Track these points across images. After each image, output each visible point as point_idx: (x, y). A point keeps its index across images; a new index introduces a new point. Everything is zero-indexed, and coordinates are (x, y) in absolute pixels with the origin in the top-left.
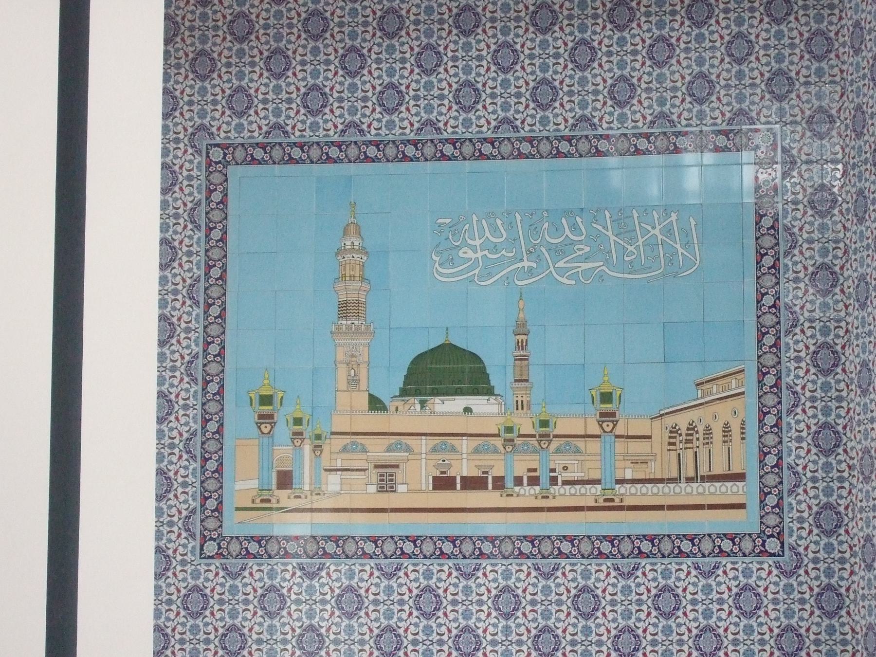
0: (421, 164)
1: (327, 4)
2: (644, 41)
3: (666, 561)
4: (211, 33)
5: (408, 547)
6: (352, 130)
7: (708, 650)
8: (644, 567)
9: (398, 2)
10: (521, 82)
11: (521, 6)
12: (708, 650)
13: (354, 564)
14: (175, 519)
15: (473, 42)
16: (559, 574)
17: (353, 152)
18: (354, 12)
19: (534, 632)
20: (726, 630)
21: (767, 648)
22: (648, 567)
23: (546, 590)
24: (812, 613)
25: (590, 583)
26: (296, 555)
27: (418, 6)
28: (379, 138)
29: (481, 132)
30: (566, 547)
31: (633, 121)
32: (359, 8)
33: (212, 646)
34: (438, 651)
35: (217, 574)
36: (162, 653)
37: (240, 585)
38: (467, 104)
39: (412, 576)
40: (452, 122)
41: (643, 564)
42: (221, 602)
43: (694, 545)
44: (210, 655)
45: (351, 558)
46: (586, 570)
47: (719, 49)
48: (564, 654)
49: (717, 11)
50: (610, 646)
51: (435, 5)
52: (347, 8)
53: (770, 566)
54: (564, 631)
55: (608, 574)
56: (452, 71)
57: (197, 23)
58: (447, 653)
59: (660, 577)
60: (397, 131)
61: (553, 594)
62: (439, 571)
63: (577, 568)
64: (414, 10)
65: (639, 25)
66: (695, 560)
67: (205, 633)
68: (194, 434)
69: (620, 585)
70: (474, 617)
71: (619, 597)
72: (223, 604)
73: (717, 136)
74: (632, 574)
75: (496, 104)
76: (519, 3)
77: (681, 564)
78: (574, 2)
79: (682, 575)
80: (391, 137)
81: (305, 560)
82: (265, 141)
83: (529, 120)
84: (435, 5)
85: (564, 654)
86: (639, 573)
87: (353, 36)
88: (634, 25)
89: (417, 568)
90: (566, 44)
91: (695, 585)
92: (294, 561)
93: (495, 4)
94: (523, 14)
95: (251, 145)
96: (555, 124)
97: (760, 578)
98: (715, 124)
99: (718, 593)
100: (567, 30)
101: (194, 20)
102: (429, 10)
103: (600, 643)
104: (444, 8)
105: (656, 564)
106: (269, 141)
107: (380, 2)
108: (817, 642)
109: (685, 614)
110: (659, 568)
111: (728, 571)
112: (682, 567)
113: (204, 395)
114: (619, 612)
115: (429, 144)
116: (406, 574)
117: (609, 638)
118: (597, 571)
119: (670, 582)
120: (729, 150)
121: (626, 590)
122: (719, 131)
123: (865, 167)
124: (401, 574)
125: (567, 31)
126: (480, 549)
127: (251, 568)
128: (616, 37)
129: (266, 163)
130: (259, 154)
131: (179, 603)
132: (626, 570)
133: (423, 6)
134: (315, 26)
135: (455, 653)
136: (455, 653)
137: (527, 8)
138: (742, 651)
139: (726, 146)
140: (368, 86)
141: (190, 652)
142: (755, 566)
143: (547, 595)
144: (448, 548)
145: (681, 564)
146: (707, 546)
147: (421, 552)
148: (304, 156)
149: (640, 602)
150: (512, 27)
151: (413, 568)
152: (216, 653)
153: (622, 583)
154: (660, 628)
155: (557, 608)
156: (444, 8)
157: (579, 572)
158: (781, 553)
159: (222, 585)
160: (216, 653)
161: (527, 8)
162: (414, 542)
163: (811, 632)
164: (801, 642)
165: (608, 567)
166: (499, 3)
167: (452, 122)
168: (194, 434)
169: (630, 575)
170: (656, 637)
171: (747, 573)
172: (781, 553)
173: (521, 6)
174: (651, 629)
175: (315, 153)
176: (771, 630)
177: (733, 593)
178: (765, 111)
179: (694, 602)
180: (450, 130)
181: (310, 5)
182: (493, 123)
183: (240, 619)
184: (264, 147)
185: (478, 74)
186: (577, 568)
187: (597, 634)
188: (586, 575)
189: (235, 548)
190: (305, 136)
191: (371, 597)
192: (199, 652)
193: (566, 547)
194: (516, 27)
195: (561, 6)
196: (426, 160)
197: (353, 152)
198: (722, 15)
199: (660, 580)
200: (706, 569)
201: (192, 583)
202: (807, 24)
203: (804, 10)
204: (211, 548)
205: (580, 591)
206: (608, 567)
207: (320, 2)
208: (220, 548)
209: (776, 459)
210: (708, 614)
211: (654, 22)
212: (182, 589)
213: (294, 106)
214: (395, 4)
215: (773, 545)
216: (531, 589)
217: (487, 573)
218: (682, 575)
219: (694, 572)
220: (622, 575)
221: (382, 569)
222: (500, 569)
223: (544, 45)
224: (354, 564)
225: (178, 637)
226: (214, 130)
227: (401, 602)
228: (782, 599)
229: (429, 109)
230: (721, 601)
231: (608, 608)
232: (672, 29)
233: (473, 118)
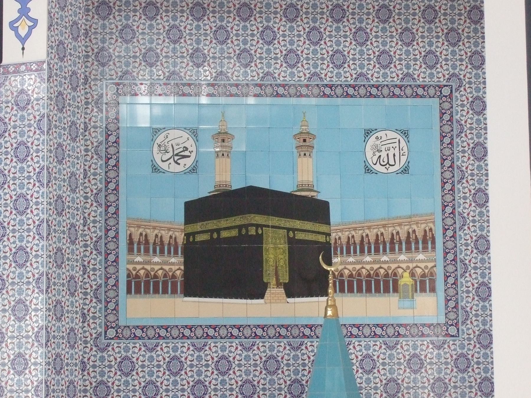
0: (381, 99)
1: (436, 2)
2: (285, 382)
3: (223, 341)
4: (457, 18)
5: (211, 332)
6: (315, 77)
7: (296, 394)
8: (354, 343)
9: (388, 1)
10: (324, 51)
11: (184, 4)
12: (296, 394)
13: (178, 343)
14: (91, 370)
15: (341, 26)
16: (110, 349)
17: (409, 91)
18: (407, 7)
19: (288, 383)
20: (162, 383)
21: (283, 392)
22: (213, 345)
23: (199, 358)
24: (261, 372)
25: (129, 354)
26: (428, 336)
27: (308, 3)
28: (425, 83)
29: (347, 81)
31: (298, 77)
32: (410, 4)
33: (379, 391)
34: (230, 395)
35: (189, 349)
36: (396, 395)
37: (106, 356)
39: (358, 348)
40: (329, 74)
41: (306, 342)
42: (207, 366)
43: (191, 332)
44: (378, 396)
45: (127, 339)
46: (126, 346)
47: (162, 34)
48: (259, 396)
49: (161, 11)
50: (286, 391)
51: (318, 3)
52: (449, 5)
53: (140, 345)
54: (162, 383)
55: (140, 349)
56: (236, 43)
57: (449, 11)
58: (284, 395)
60: (389, 79)
61: (300, 360)
62: (374, 345)
63: (218, 344)
64: (305, 6)
65: (161, 18)
66: (240, 340)
67: (469, 382)
69: (243, 355)
70: (106, 375)
71: (243, 362)
72: (192, 367)
73: (255, 87)
74: (299, 348)
75: (356, 64)
76: (183, 2)
77: (232, 342)
78: (122, 2)
79: (136, 350)
80: (339, 83)
81: (434, 338)
82: (401, 83)
83: (329, 74)
84: (318, 3)
85: (259, 396)
86: (207, 348)
87: (407, 21)
88: (206, 18)
89: (217, 345)
90: (304, 29)
92: (428, 339)
93: (261, 3)
94: (232, 9)
95: (346, 86)
96: (345, 77)
98: (112, 79)
99: (157, 361)
100: (305, 21)
101: (215, 7)
102: (315, 6)
103: (231, 390)
104: (324, 5)
105: (169, 343)
107: (423, 1)
108: (215, 390)
109: (137, 373)
110: (171, 345)
112: (377, 343)
114: (146, 372)
115: (339, 87)
116: (113, 349)
117: (189, 387)
118: (374, 345)
119: (197, 354)
120: (262, 96)
121: (247, 358)
122: (256, 84)
124: (207, 348)
125: (259, 20)
126: (374, 332)
127: (162, 345)
128: (288, 26)
129: (379, 97)
130: (351, 91)
131: (186, 366)
132: (296, 346)
133: (311, 3)
134: (383, 14)
135: (288, 396)
136: (288, 396)
137: (188, 5)
138: (268, 395)
139: (213, 93)
141: (365, 395)
142: (276, 345)
143: (200, 361)
144: (187, 332)
145: (280, 342)
146: (199, 332)
148: (379, 93)
149: (256, 365)
150: (365, 19)
151: (262, 344)
152: (381, 395)
153: (245, 353)
154: (122, 382)
156: (324, 5)
158: (457, 335)
159: (384, 354)
160: (381, 395)
161: (188, 5)
162: (239, 329)
163: (212, 384)
164: (158, 391)
165: (285, 344)
166: (218, 2)
167: (329, 74)
169: (249, 349)
170: (120, 387)
171: (367, 348)
172: (457, 335)
173: (184, 4)
174: (117, 383)
175: (386, 91)
176: (476, 380)
178: (141, 72)
179: (94, 366)
180: (328, 79)
181: (472, 2)
182: (354, 76)
183: (106, 377)
184: (354, 87)
185: (298, 46)
186: (218, 344)
187: (278, 384)
188: (127, 350)
190: (426, 81)
191: (475, 360)
192: (371, 395)
193: (163, 333)
194: (274, 18)
195: (114, 4)
196: (384, 97)
197: (409, 91)
198: (117, 13)
199: (220, 352)
200: (248, 346)
201: (394, 352)
202: (168, 21)
203: (306, 15)
204: (452, 330)
206: (189, 345)
207: (477, 1)
209: (454, 279)
210: (247, 373)
211: (310, 18)
212: (359, 356)
214: (386, 3)
215: (111, 333)
216: (476, 355)
217: (212, 348)
219: (288, 347)
220: (293, 348)
221: (434, 344)
222: (411, 343)
223: (245, 28)
224: (178, 343)
225: (261, 386)
226: (416, 76)
227: (159, 366)
229: (315, 66)
230: (240, 365)
231: (189, 369)
232: (228, 22)
233: (296, 72)
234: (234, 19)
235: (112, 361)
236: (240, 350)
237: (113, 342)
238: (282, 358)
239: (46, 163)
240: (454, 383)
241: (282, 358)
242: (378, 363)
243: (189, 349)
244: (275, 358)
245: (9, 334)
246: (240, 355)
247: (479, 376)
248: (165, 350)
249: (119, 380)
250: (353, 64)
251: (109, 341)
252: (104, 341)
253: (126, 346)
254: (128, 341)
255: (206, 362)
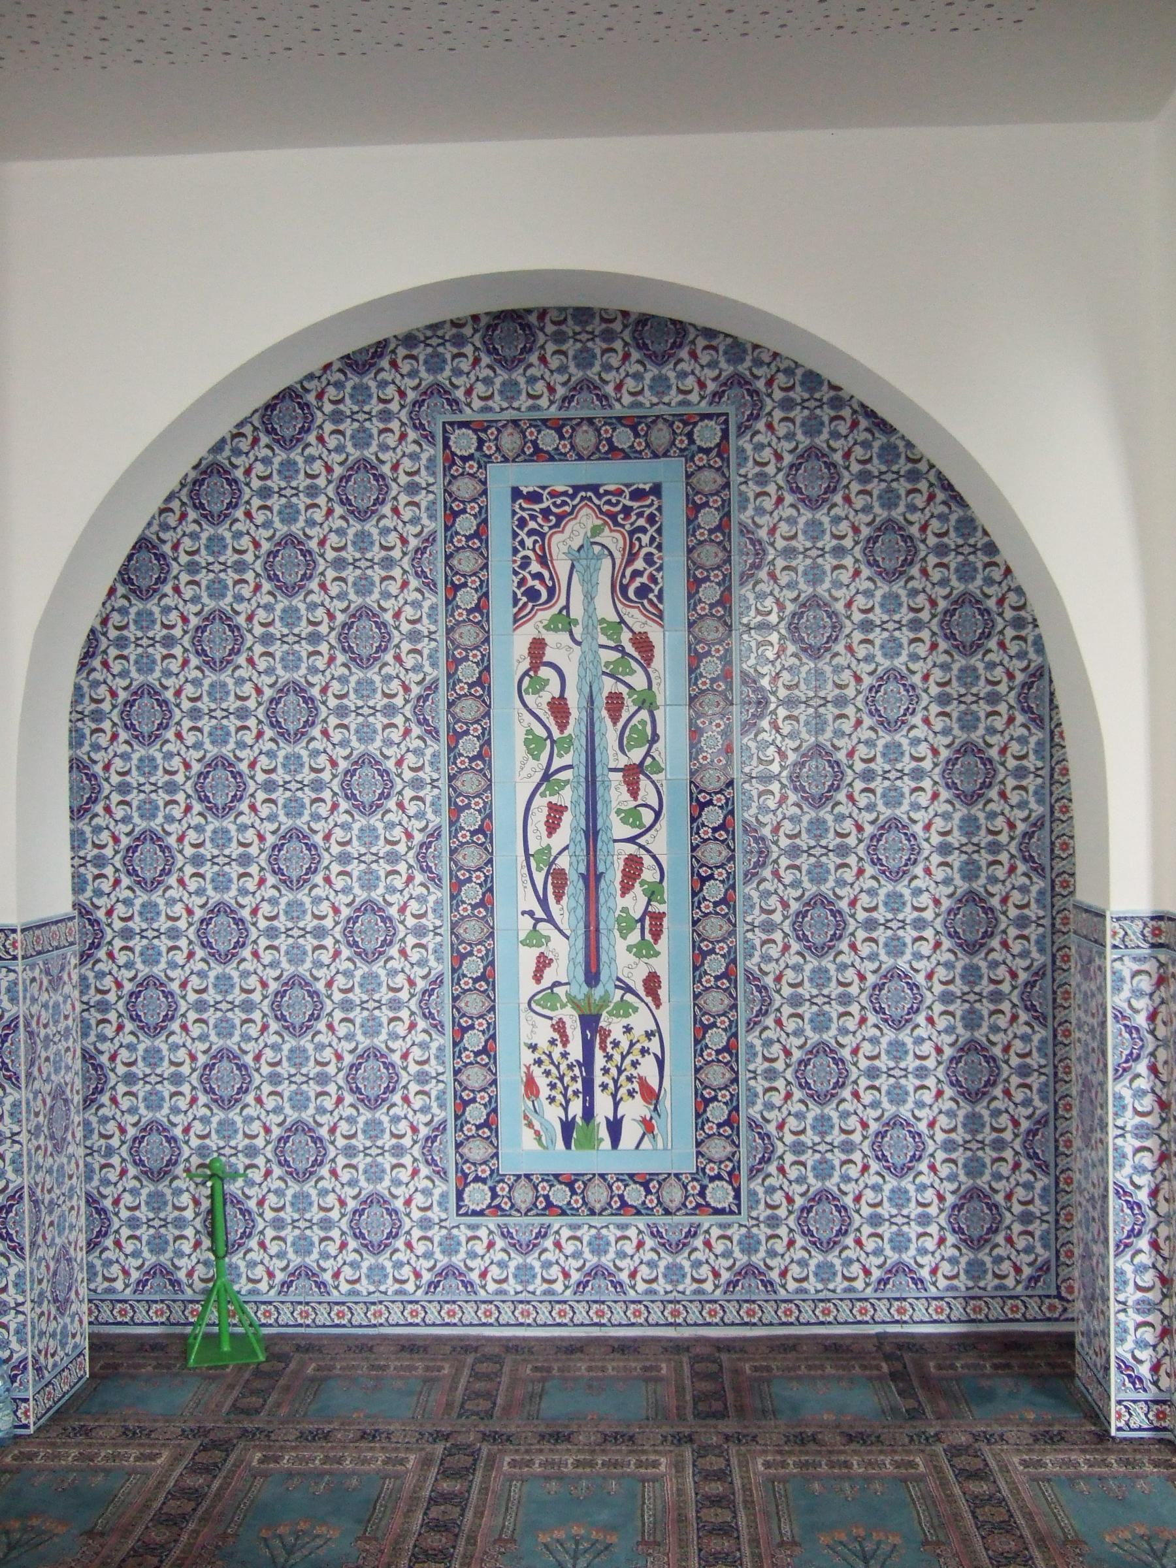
5: (475, 1040)
30: (469, 746)
35: (178, 693)
38: (365, 652)
59: (989, 1265)
68: (436, 834)
79: (332, 1249)
91: (394, 1036)
97: (279, 1193)
106: (571, 413)
111: (266, 1278)
113: (726, 503)
123: (53, 1195)
140: (174, 617)
147: (466, 1065)
155: (130, 924)
157: (839, 1278)
168: (436, 834)
169: (530, 1247)
177: (418, 989)
187: (202, 876)
189: (718, 1149)
205: (155, 591)
208: (719, 1177)
213: (254, 869)
218: (480, 1248)
228: (1032, 769)
234: (477, 361)
235: (265, 801)
236: (241, 760)
237: (704, 407)
238: (186, 1130)
239: (26, 1180)
240: (123, 919)
241: (330, 512)
242: (185, 1147)
243: (178, 693)
244: (279, 588)
245: (774, 637)
246: (239, 598)
247: (789, 446)
248: (569, 1248)
249: (173, 965)
250: (178, 919)
251: (713, 410)
252: (731, 410)
253: (598, 1237)
254: (657, 411)
255: (241, 850)
